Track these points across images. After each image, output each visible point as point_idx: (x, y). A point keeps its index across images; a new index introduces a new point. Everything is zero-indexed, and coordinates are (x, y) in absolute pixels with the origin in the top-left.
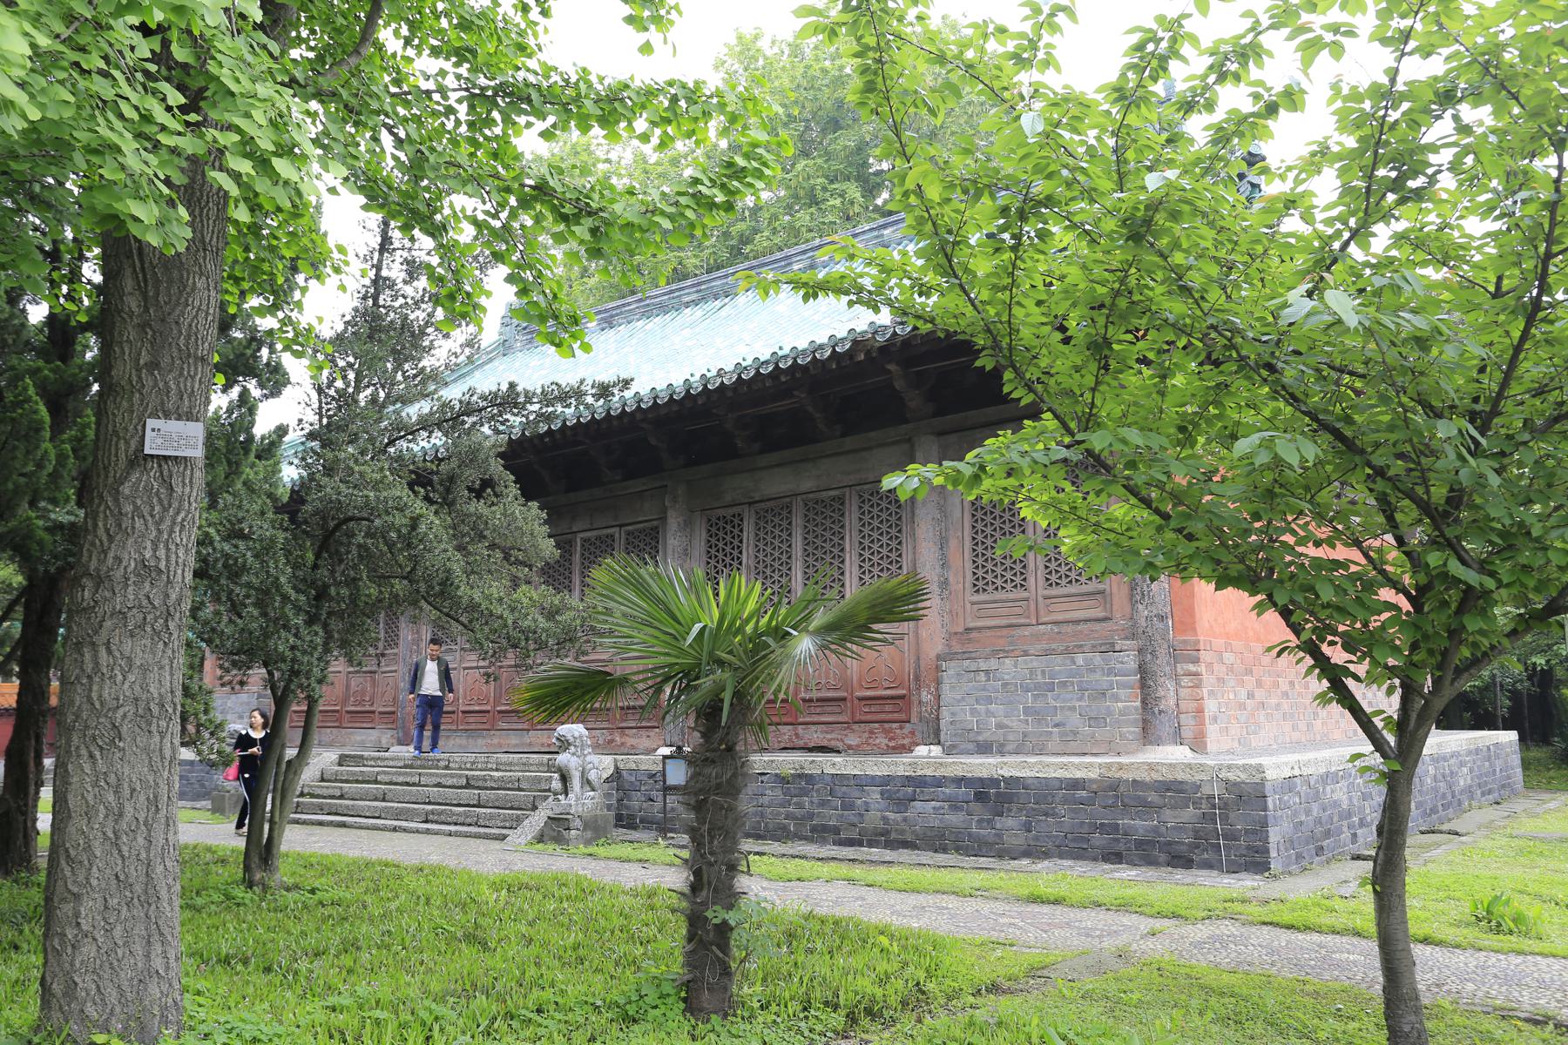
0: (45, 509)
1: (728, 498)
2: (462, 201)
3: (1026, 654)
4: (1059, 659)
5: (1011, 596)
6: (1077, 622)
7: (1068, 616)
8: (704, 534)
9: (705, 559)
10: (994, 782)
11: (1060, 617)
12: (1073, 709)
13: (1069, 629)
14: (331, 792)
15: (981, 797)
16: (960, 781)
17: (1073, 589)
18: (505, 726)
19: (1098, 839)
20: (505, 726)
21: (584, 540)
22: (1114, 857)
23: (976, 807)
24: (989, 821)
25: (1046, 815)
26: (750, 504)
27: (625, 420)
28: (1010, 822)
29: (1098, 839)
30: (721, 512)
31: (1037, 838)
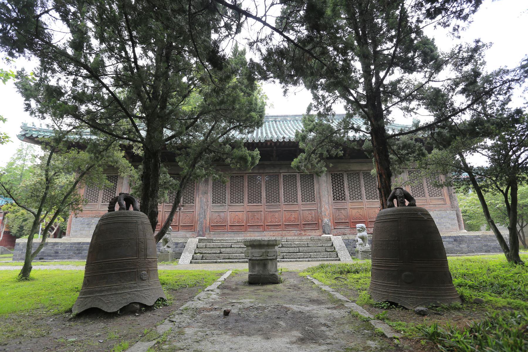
0: (376, 29)
1: (340, 169)
2: (339, 31)
3: (435, 211)
4: (443, 212)
5: (421, 198)
6: (439, 204)
7: (436, 203)
8: (331, 178)
9: (331, 184)
10: (458, 237)
11: (434, 203)
12: (447, 222)
13: (437, 206)
14: (214, 252)
15: (455, 240)
16: (450, 237)
17: (436, 198)
18: (251, 230)
19: (484, 248)
20: (251, 230)
21: (284, 176)
22: (488, 251)
23: (455, 243)
24: (459, 246)
25: (472, 243)
26: (345, 171)
27: (278, 144)
28: (464, 246)
29: (484, 248)
30: (336, 172)
31: (470, 249)
